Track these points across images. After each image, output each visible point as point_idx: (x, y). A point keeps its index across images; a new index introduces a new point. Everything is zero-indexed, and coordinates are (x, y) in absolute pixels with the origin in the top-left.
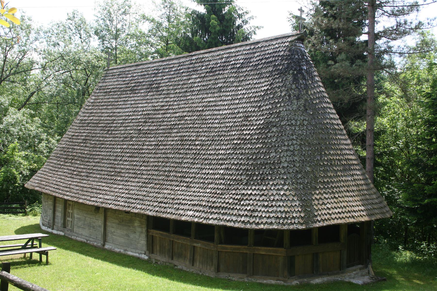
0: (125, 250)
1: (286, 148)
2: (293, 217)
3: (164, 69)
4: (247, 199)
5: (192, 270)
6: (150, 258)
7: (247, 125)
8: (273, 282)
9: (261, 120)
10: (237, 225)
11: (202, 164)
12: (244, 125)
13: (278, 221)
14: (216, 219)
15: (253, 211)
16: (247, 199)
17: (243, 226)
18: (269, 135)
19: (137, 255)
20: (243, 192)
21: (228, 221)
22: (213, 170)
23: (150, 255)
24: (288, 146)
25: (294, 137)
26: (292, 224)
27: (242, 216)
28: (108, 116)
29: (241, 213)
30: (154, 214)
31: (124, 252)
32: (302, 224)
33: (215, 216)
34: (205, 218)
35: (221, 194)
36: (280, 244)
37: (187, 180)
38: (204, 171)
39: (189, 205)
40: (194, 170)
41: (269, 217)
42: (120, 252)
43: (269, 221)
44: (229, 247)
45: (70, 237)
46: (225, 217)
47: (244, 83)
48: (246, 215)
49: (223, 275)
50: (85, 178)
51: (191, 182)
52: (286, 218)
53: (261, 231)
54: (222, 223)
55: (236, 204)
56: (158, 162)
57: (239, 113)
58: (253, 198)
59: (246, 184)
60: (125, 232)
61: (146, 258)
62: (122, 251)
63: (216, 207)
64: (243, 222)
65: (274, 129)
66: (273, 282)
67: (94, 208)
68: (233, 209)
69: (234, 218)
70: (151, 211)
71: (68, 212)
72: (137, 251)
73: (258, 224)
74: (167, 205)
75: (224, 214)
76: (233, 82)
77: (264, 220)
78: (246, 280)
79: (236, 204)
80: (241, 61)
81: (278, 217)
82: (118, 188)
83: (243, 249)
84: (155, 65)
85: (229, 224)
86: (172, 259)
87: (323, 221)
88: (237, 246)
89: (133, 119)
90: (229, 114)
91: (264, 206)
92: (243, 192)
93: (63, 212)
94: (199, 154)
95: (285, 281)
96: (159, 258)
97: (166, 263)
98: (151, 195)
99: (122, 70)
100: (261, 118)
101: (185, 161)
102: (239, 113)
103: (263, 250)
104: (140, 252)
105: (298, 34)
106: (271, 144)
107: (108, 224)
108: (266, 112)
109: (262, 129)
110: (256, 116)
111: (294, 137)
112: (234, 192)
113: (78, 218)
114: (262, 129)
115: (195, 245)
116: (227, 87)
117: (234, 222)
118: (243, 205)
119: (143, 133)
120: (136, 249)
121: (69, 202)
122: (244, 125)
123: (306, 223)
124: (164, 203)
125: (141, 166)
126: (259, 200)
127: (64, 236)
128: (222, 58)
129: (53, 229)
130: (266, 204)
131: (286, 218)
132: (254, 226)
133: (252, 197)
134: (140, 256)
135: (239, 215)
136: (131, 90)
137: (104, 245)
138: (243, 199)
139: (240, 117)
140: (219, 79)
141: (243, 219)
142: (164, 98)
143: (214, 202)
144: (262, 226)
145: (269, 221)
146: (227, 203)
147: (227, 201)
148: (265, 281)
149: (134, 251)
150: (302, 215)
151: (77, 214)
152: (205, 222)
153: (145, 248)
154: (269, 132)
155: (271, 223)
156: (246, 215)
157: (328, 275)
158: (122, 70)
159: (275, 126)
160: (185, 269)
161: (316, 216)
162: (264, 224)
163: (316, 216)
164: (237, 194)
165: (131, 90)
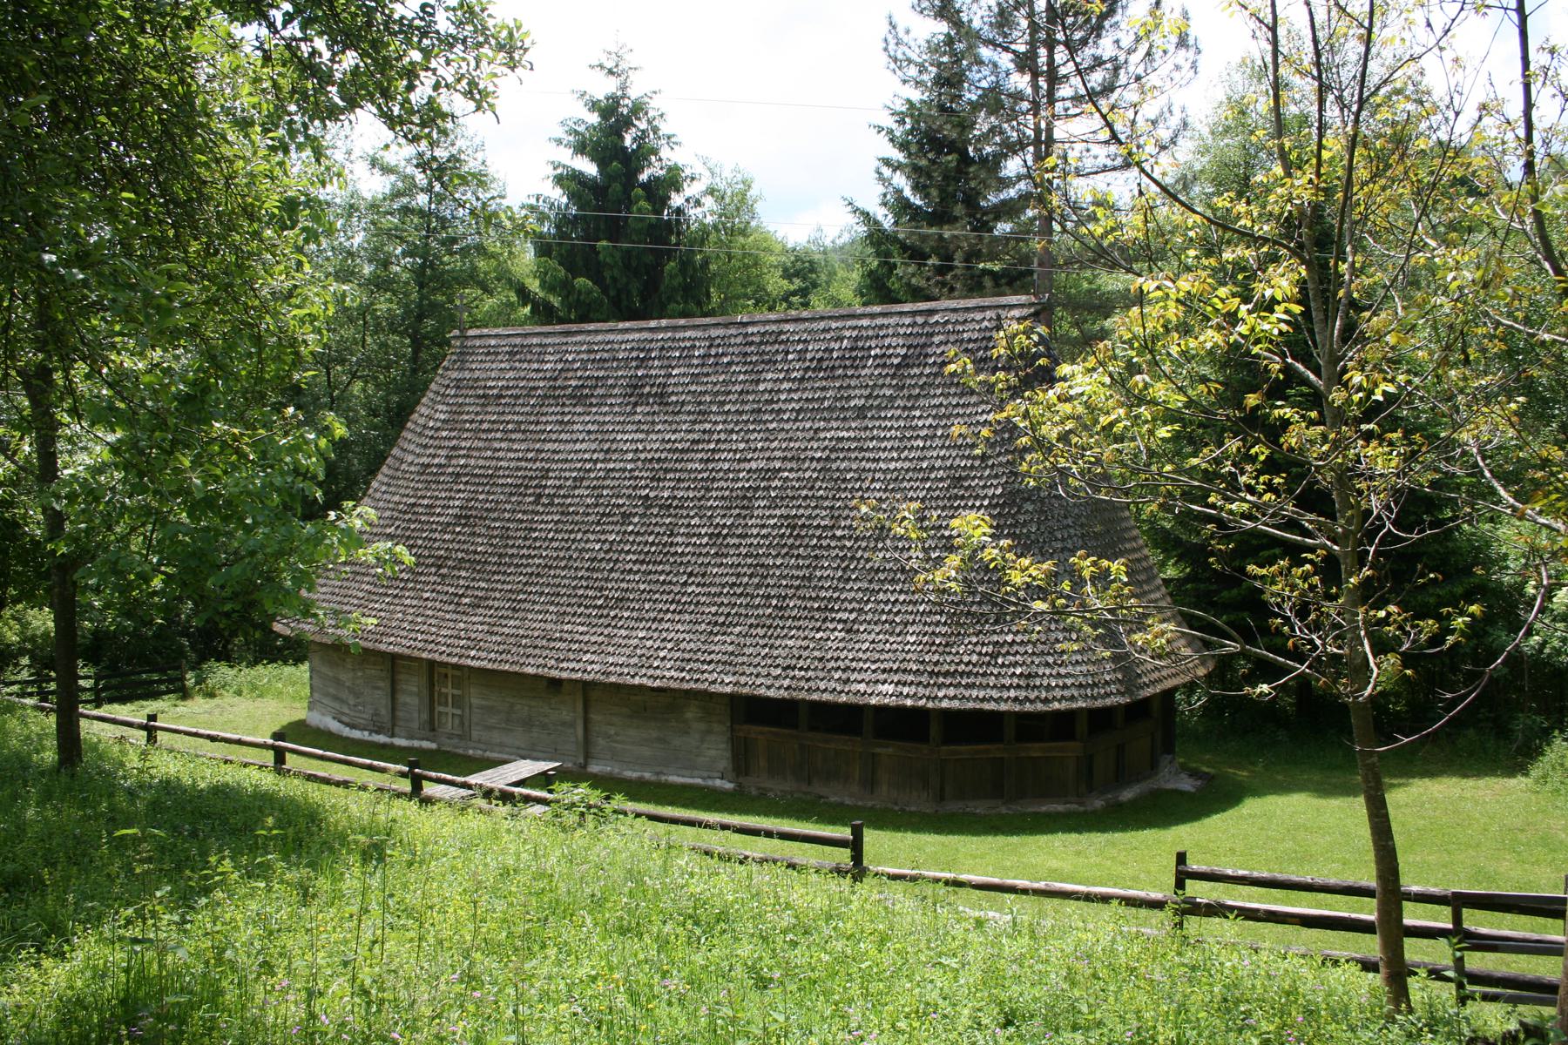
0: (658, 774)
1: (1059, 545)
2: (1107, 683)
3: (662, 348)
4: (1008, 653)
5: (870, 804)
6: (740, 785)
7: (963, 497)
8: (1060, 808)
9: (996, 487)
10: (1003, 707)
11: (871, 582)
12: (956, 497)
13: (1082, 692)
14: (955, 697)
15: (1029, 676)
16: (1008, 653)
17: (1017, 708)
18: (1021, 518)
19: (699, 781)
20: (995, 638)
21: (983, 700)
22: (906, 593)
23: (741, 779)
24: (1063, 540)
25: (1070, 521)
26: (1107, 695)
27: (1008, 689)
28: (519, 459)
29: (1007, 682)
30: (783, 694)
31: (654, 778)
32: (1122, 694)
33: (951, 692)
34: (928, 698)
35: (947, 645)
36: (1070, 735)
37: (845, 616)
38: (881, 596)
39: (874, 671)
40: (853, 594)
41: (1065, 687)
42: (641, 778)
43: (1067, 693)
44: (964, 750)
45: (460, 751)
46: (975, 693)
47: (921, 402)
48: (1018, 686)
49: (953, 806)
50: (510, 613)
51: (854, 621)
52: (1095, 685)
53: (1057, 713)
54: (971, 705)
55: (989, 664)
56: (738, 575)
57: (933, 468)
58: (1022, 650)
59: (996, 622)
60: (655, 734)
61: (729, 786)
62: (647, 775)
63: (946, 674)
64: (1016, 699)
65: (1029, 507)
66: (1060, 808)
67: (545, 683)
68: (984, 674)
69: (995, 694)
70: (769, 688)
71: (440, 694)
72: (696, 773)
73: (1046, 701)
74: (810, 673)
75: (968, 686)
76: (892, 398)
77: (1058, 693)
78: (1004, 810)
79: (989, 664)
80: (903, 352)
81: (1081, 685)
82: (477, 622)
83: (994, 750)
84: (631, 337)
85: (987, 706)
86: (809, 784)
87: (1153, 683)
88: (981, 747)
89: (613, 470)
90: (907, 470)
91: (1047, 664)
92: (995, 638)
93: (425, 692)
94: (853, 558)
95: (1081, 804)
96: (768, 784)
97: (792, 793)
98: (748, 651)
99: (518, 341)
100: (995, 482)
101: (818, 574)
102: (933, 468)
103: (1036, 750)
104: (706, 774)
105: (1033, 304)
106: (1028, 537)
107: (594, 717)
108: (1001, 470)
109: (1003, 506)
110: (980, 478)
111: (1070, 521)
112: (974, 640)
113: (481, 707)
114: (1003, 506)
115: (878, 750)
116: (879, 408)
117: (1021, 702)
118: (1003, 665)
119: (661, 507)
120: (694, 768)
121: (443, 670)
122: (956, 497)
123: (1128, 691)
124: (801, 669)
125: (685, 584)
126: (1034, 653)
127: (438, 751)
128: (841, 339)
129: (393, 736)
130: (1050, 660)
131: (1095, 685)
132: (1040, 707)
133: (1015, 648)
134: (710, 783)
135: (1003, 686)
136: (571, 397)
137: (585, 766)
138: (999, 653)
139: (942, 479)
140: (849, 386)
141: (1012, 693)
142: (694, 422)
143: (937, 663)
144: (1056, 705)
145: (1067, 693)
146: (967, 664)
147: (966, 659)
148: (1044, 809)
149: (687, 773)
150: (1120, 676)
151: (476, 697)
152: (930, 705)
153: (724, 764)
154: (1018, 511)
155: (1072, 698)
156: (1018, 686)
157: (1138, 781)
158: (518, 341)
159: (1029, 499)
160: (848, 801)
161: (1139, 676)
162: (1059, 701)
163: (1139, 676)
164: (983, 644)
165: (571, 397)
